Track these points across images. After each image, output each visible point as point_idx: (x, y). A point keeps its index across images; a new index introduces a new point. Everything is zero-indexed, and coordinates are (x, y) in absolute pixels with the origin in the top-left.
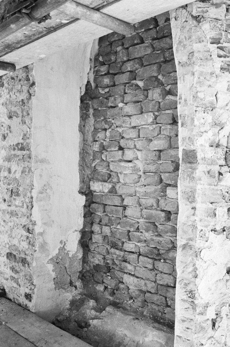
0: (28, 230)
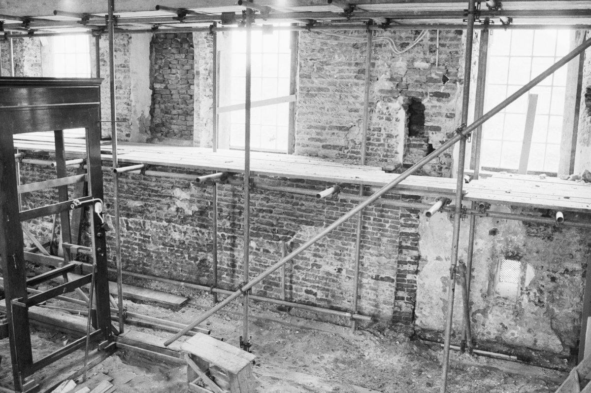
0: (128, 104)
